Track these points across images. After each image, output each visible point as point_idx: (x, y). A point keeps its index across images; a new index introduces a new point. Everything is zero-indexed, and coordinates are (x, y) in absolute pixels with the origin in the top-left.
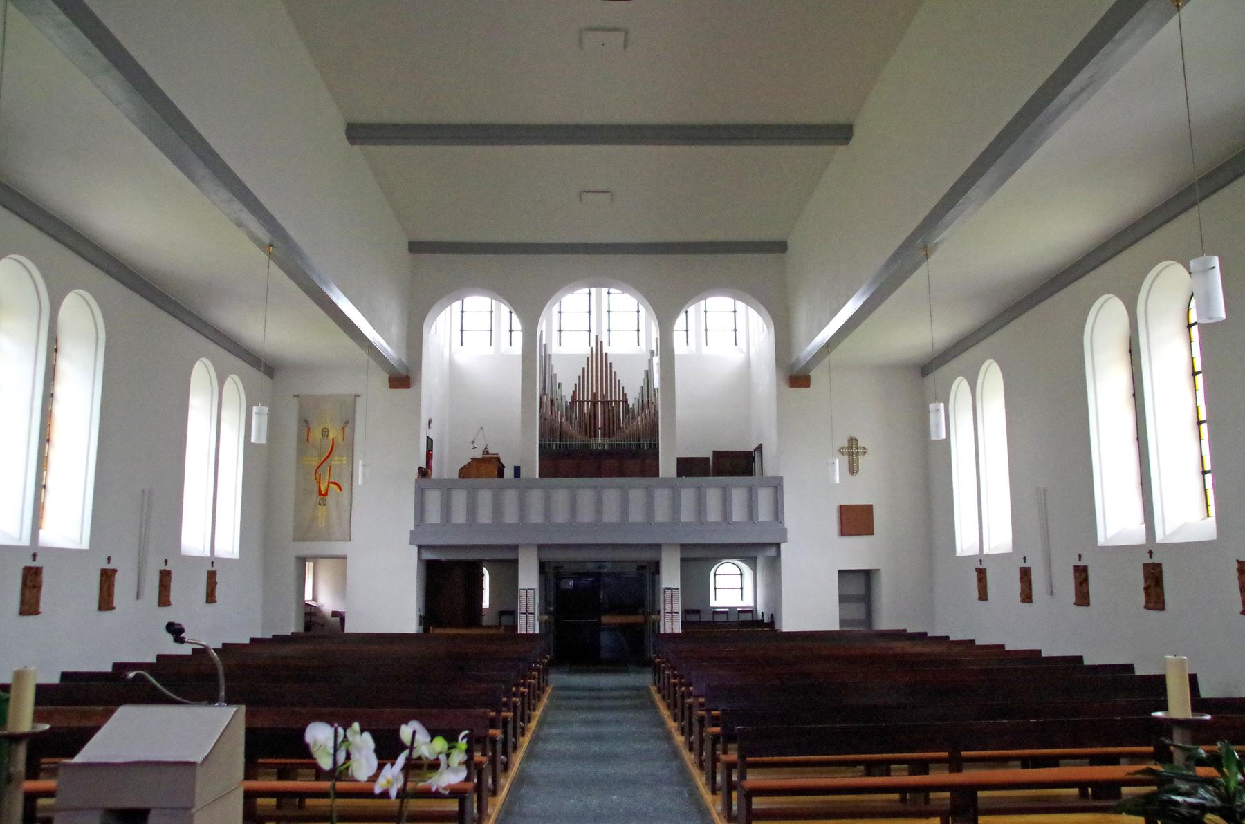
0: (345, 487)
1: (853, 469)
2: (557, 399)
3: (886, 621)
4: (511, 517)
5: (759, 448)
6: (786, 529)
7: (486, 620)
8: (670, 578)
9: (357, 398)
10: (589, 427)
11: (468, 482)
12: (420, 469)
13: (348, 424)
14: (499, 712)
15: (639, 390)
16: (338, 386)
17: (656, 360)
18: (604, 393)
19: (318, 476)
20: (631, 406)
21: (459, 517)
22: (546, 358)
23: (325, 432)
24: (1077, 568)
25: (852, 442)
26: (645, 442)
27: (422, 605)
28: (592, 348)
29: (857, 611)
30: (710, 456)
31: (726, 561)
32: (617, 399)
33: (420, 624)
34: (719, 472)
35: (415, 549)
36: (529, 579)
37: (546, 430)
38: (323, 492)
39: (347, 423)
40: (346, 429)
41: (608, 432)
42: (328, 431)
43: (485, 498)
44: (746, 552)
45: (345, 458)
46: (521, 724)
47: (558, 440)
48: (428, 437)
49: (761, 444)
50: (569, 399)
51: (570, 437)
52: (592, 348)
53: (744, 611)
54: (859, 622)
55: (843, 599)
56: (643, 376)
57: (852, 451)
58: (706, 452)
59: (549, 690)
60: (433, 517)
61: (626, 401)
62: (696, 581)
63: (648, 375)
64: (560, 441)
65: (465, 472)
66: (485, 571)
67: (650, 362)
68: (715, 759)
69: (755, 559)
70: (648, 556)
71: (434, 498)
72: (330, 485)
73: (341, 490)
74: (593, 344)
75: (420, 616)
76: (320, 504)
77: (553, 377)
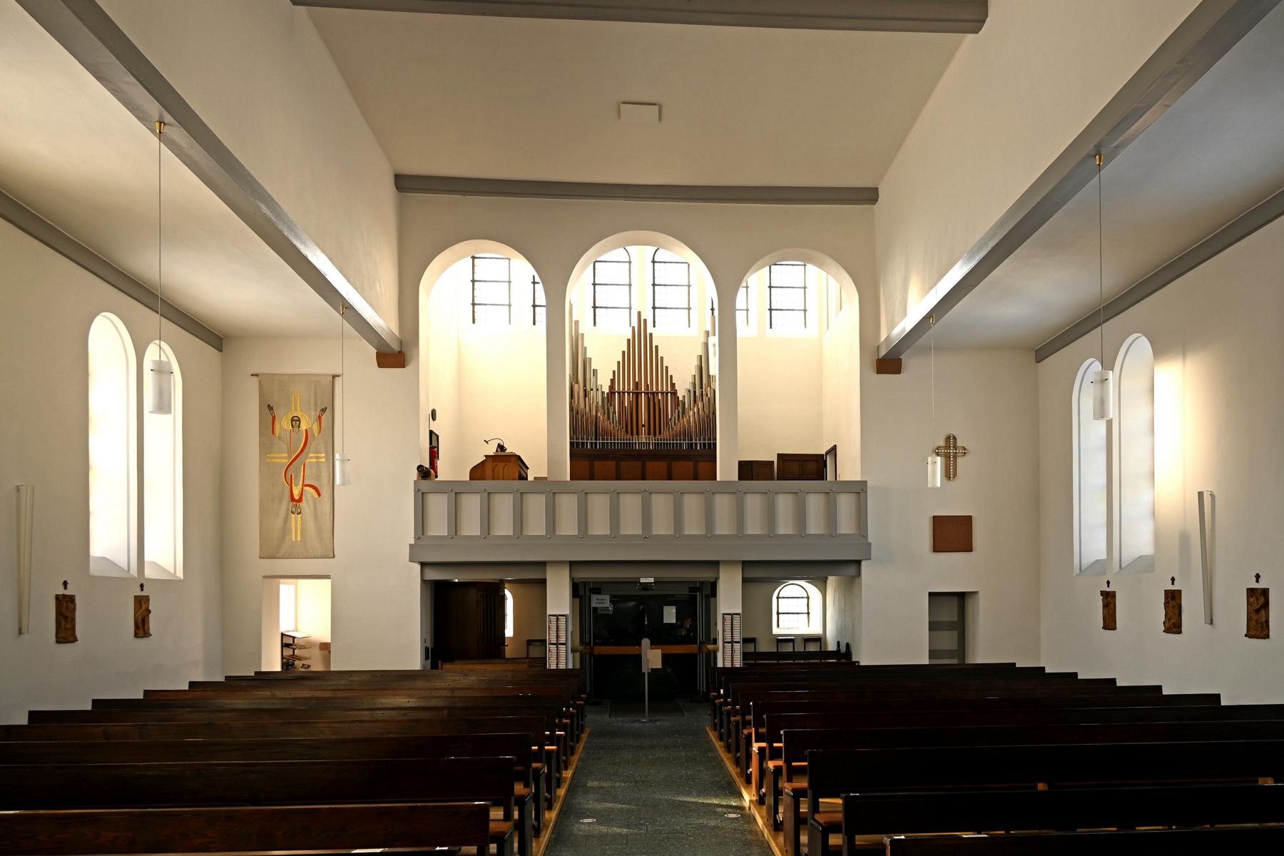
0: (325, 491)
1: (949, 473)
2: (592, 390)
3: (983, 653)
4: (536, 527)
5: (833, 450)
6: (870, 544)
7: (509, 653)
8: (729, 599)
9: (337, 378)
10: (631, 425)
11: (488, 484)
12: (420, 468)
13: (325, 411)
14: (541, 746)
15: (690, 380)
16: (318, 363)
17: (714, 340)
18: (649, 383)
19: (289, 478)
20: (681, 399)
21: (471, 527)
22: (577, 340)
23: (295, 421)
24: (1251, 592)
25: (951, 440)
26: (698, 443)
27: (428, 636)
28: (634, 328)
29: (948, 640)
30: (775, 459)
31: (791, 582)
32: (665, 390)
33: (427, 658)
34: (782, 476)
35: (418, 567)
36: (559, 601)
37: (581, 425)
38: (297, 498)
39: (324, 410)
40: (323, 418)
41: (653, 429)
42: (299, 420)
43: (504, 505)
44: (815, 570)
45: (323, 455)
46: (571, 743)
47: (594, 437)
48: (431, 432)
49: (835, 446)
50: (606, 390)
51: (606, 433)
52: (634, 328)
53: (808, 639)
54: (950, 654)
55: (933, 626)
56: (695, 362)
57: (950, 451)
58: (768, 454)
59: (584, 737)
60: (439, 527)
61: (674, 393)
62: (758, 610)
63: (702, 368)
64: (596, 439)
65: (478, 472)
66: (507, 593)
67: (706, 345)
68: (778, 793)
69: (825, 581)
70: (703, 575)
71: (438, 505)
72: (305, 488)
73: (319, 495)
74: (635, 323)
75: (427, 649)
76: (292, 512)
77: (586, 362)
